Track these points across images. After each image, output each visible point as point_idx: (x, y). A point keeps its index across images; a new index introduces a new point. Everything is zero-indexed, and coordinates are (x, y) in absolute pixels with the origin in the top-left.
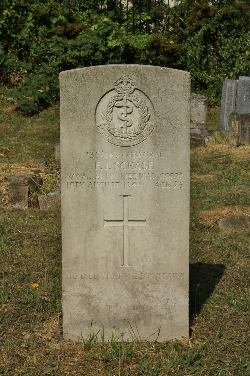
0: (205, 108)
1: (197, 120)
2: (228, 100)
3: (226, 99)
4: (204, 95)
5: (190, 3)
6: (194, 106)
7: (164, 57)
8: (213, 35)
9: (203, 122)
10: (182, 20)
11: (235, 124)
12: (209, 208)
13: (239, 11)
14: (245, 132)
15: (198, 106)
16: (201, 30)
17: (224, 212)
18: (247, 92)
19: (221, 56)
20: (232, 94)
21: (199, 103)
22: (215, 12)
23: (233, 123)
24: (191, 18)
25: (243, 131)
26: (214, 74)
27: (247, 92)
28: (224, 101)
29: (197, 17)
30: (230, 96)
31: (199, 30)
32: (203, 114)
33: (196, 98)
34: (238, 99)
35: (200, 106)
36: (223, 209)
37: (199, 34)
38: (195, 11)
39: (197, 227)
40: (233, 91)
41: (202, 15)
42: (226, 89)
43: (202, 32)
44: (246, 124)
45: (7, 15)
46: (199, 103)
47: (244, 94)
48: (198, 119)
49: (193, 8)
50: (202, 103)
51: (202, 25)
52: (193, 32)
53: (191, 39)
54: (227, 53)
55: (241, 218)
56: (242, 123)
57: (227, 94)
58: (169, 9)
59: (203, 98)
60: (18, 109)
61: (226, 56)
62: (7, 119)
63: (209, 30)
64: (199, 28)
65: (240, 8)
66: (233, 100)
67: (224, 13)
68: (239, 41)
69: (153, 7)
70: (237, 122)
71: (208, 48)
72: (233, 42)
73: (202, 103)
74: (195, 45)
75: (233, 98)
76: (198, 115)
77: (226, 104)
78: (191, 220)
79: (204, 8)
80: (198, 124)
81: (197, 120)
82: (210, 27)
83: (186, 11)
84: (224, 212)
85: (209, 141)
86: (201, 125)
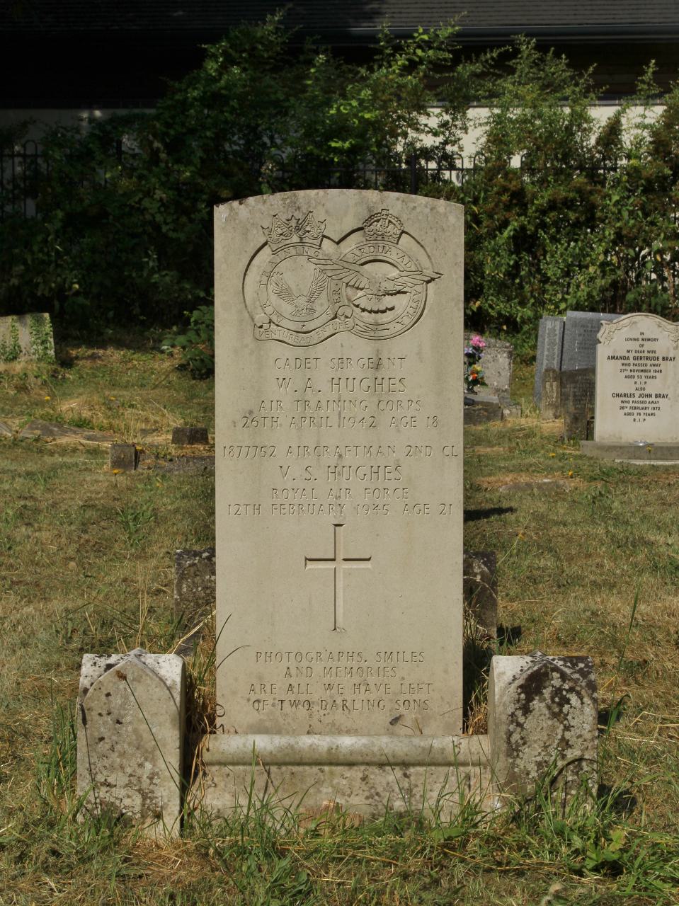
0: (510, 364)
1: (496, 384)
2: (548, 350)
3: (546, 349)
4: (508, 341)
5: (491, 180)
6: (492, 360)
7: (130, 814)
8: (530, 236)
9: (506, 387)
10: (475, 208)
11: (551, 386)
12: (490, 475)
13: (577, 196)
14: (567, 399)
15: (498, 360)
16: (509, 228)
17: (508, 479)
18: (581, 338)
19: (545, 274)
20: (555, 340)
21: (499, 356)
22: (535, 196)
23: (548, 385)
24: (491, 205)
25: (563, 397)
26: (533, 305)
27: (581, 338)
28: (543, 352)
29: (501, 205)
30: (552, 343)
31: (506, 228)
32: (506, 374)
33: (495, 346)
34: (564, 349)
35: (501, 360)
36: (507, 476)
37: (506, 234)
38: (499, 193)
39: (471, 488)
40: (556, 335)
41: (511, 201)
42: (544, 332)
43: (511, 231)
44: (568, 386)
45: (161, 200)
46: (499, 356)
47: (575, 340)
48: (498, 382)
49: (495, 189)
50: (505, 355)
51: (510, 219)
52: (494, 230)
53: (490, 243)
54: (556, 269)
55: (527, 484)
56: (562, 385)
57: (547, 340)
58: (453, 189)
59: (506, 347)
60: (182, 368)
61: (555, 275)
62: (163, 383)
63: (523, 228)
64: (505, 224)
65: (579, 191)
66: (556, 351)
67: (551, 198)
68: (577, 249)
69: (422, 186)
70: (555, 384)
71: (521, 259)
72: (566, 249)
73: (505, 355)
74: (498, 254)
75: (556, 347)
76: (498, 374)
77: (545, 357)
78: (465, 479)
79: (514, 189)
80: (497, 390)
81: (496, 384)
82: (526, 223)
83: (482, 195)
84: (508, 479)
85: (511, 414)
86: (503, 391)
